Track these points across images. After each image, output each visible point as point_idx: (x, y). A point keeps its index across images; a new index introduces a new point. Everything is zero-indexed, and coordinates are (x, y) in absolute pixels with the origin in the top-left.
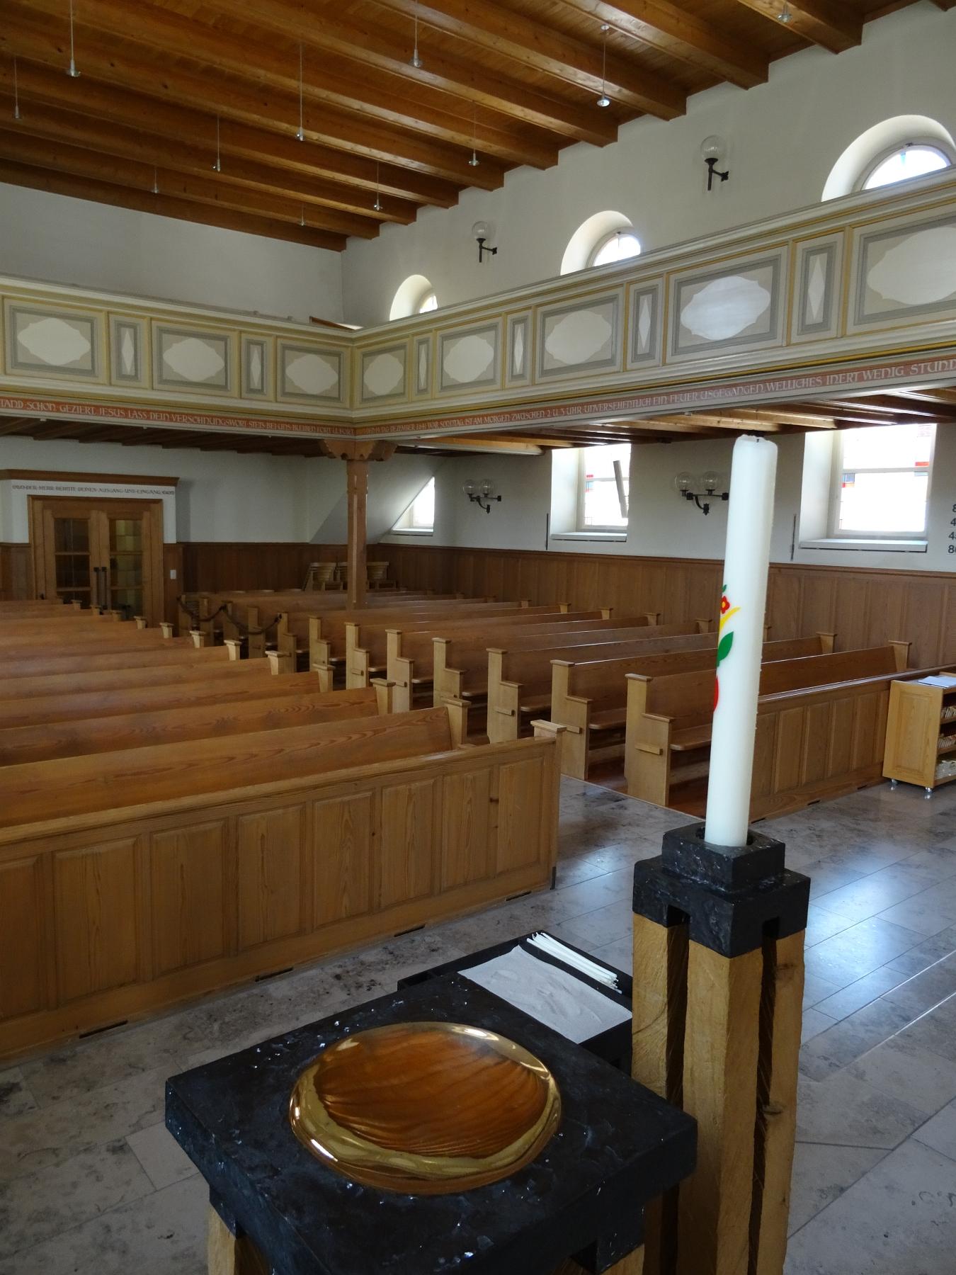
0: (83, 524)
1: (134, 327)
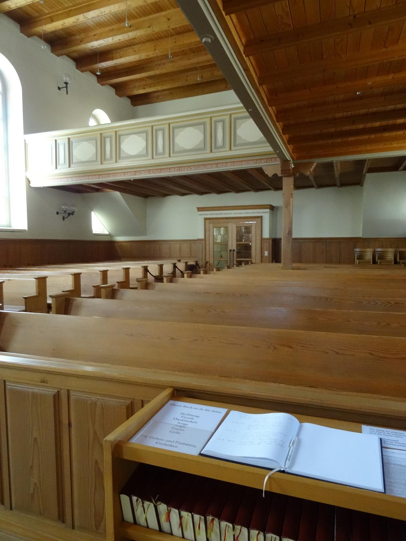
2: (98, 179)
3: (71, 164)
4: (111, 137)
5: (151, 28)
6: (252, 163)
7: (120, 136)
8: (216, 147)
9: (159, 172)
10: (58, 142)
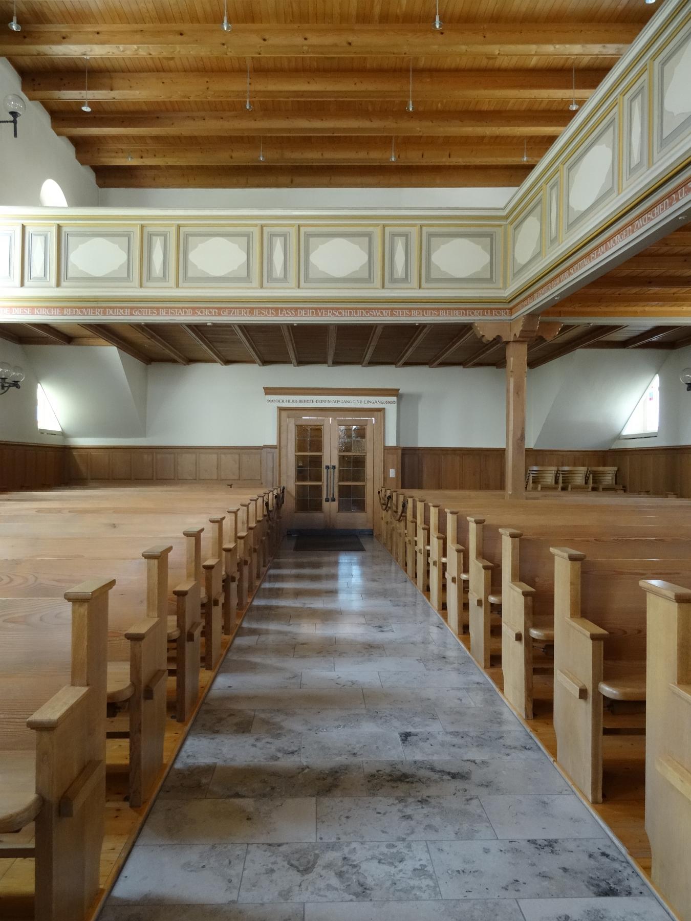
0: (317, 431)
1: (285, 236)
2: (128, 315)
3: (62, 280)
4: (165, 236)
5: (225, 47)
6: (457, 314)
7: (187, 236)
8: (271, 278)
9: (272, 313)
10: (28, 230)
